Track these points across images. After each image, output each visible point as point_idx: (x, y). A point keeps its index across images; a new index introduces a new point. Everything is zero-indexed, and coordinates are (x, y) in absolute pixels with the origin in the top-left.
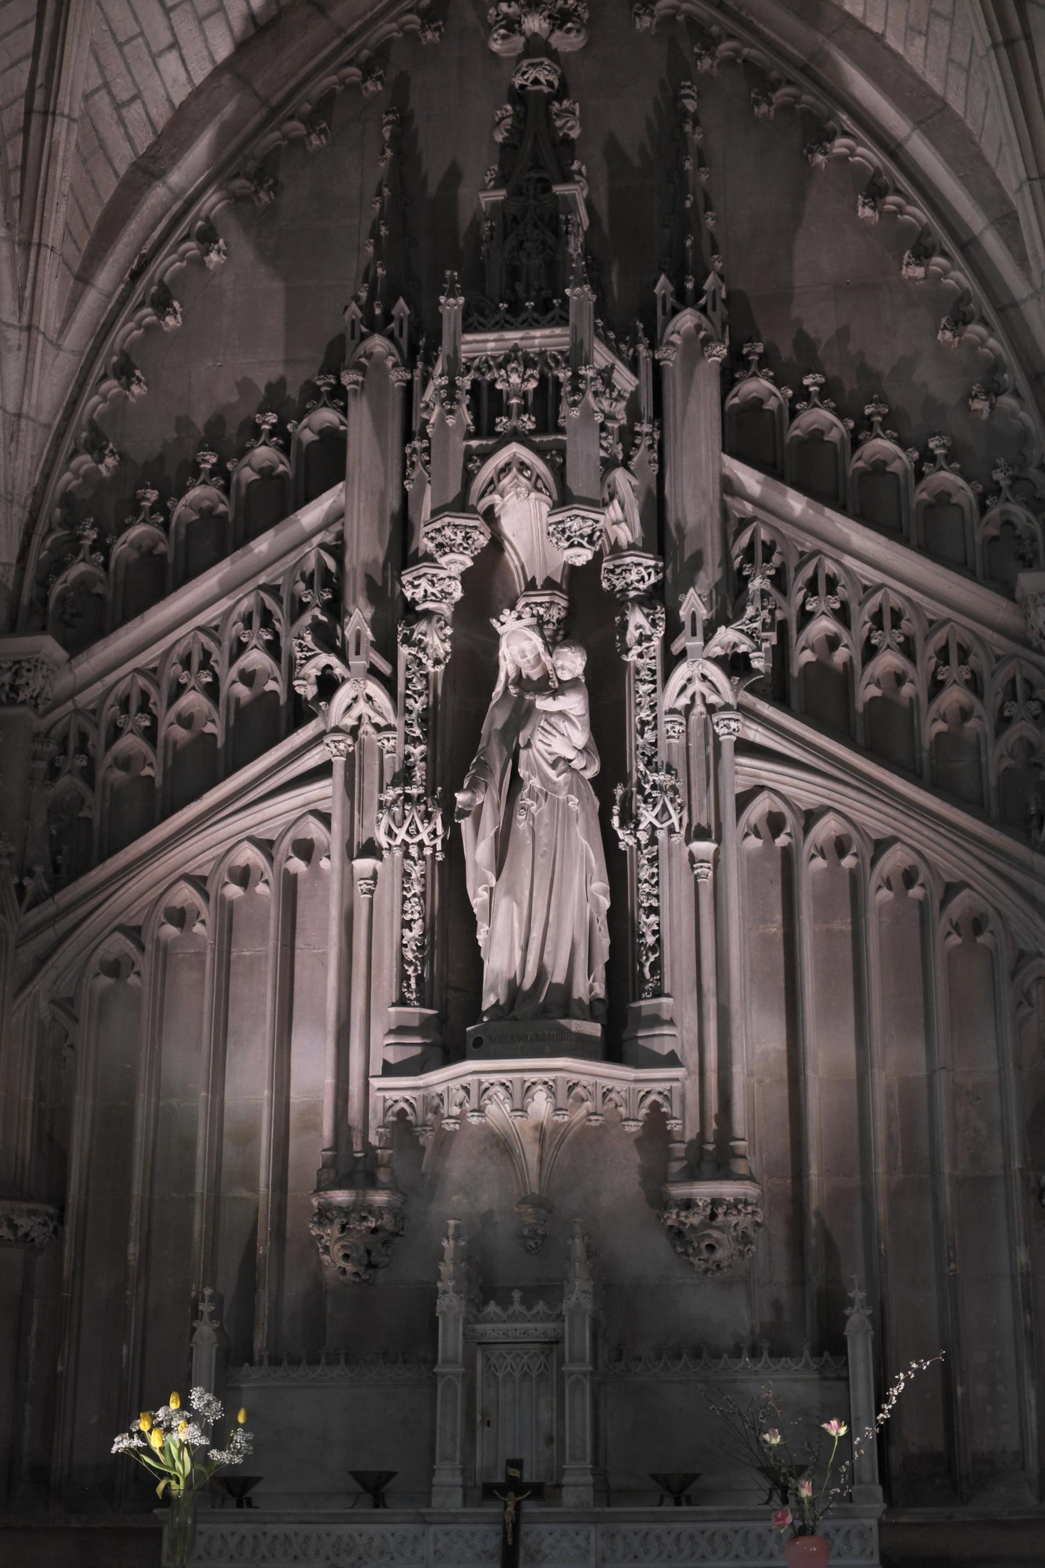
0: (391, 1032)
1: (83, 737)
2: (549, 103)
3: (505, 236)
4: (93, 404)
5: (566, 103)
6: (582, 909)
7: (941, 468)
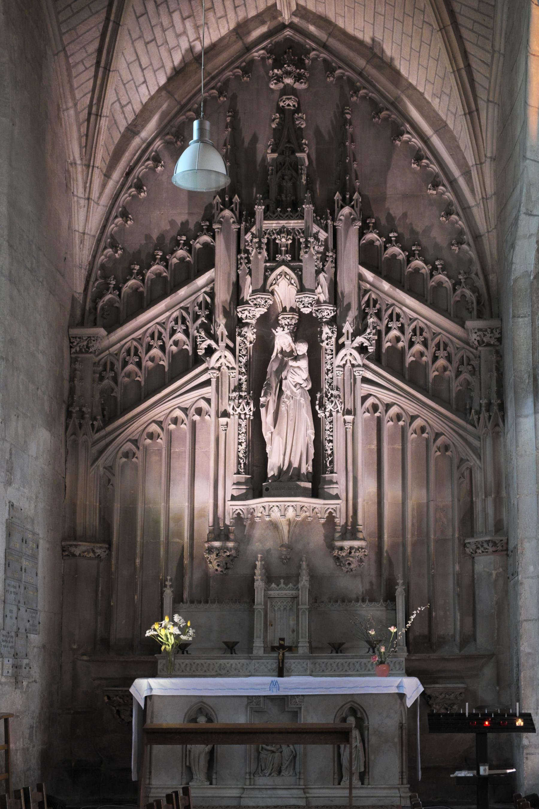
0: (234, 484)
1: (112, 364)
2: (294, 114)
3: (277, 172)
4: (112, 228)
5: (300, 114)
6: (304, 440)
7: (440, 273)
